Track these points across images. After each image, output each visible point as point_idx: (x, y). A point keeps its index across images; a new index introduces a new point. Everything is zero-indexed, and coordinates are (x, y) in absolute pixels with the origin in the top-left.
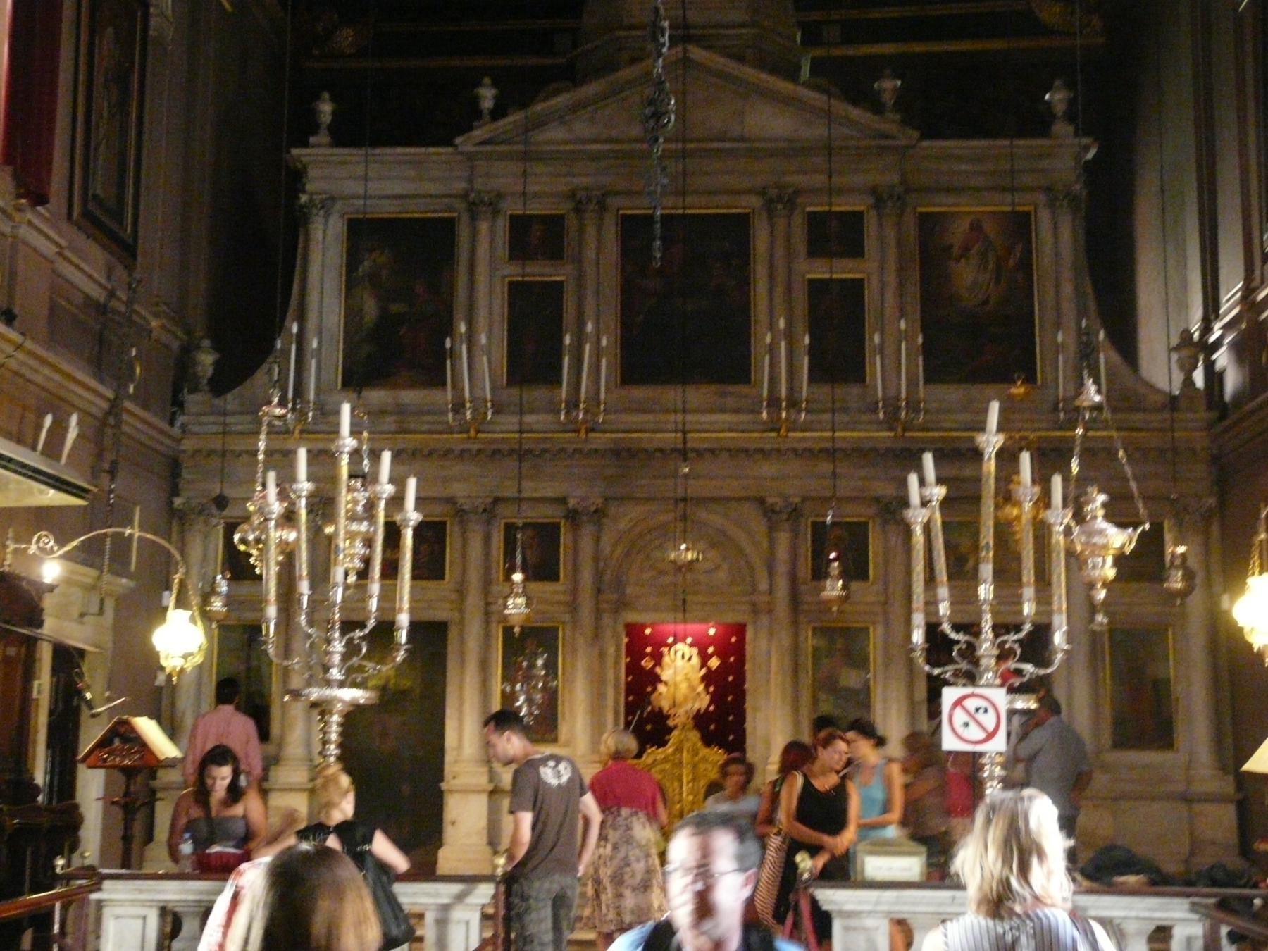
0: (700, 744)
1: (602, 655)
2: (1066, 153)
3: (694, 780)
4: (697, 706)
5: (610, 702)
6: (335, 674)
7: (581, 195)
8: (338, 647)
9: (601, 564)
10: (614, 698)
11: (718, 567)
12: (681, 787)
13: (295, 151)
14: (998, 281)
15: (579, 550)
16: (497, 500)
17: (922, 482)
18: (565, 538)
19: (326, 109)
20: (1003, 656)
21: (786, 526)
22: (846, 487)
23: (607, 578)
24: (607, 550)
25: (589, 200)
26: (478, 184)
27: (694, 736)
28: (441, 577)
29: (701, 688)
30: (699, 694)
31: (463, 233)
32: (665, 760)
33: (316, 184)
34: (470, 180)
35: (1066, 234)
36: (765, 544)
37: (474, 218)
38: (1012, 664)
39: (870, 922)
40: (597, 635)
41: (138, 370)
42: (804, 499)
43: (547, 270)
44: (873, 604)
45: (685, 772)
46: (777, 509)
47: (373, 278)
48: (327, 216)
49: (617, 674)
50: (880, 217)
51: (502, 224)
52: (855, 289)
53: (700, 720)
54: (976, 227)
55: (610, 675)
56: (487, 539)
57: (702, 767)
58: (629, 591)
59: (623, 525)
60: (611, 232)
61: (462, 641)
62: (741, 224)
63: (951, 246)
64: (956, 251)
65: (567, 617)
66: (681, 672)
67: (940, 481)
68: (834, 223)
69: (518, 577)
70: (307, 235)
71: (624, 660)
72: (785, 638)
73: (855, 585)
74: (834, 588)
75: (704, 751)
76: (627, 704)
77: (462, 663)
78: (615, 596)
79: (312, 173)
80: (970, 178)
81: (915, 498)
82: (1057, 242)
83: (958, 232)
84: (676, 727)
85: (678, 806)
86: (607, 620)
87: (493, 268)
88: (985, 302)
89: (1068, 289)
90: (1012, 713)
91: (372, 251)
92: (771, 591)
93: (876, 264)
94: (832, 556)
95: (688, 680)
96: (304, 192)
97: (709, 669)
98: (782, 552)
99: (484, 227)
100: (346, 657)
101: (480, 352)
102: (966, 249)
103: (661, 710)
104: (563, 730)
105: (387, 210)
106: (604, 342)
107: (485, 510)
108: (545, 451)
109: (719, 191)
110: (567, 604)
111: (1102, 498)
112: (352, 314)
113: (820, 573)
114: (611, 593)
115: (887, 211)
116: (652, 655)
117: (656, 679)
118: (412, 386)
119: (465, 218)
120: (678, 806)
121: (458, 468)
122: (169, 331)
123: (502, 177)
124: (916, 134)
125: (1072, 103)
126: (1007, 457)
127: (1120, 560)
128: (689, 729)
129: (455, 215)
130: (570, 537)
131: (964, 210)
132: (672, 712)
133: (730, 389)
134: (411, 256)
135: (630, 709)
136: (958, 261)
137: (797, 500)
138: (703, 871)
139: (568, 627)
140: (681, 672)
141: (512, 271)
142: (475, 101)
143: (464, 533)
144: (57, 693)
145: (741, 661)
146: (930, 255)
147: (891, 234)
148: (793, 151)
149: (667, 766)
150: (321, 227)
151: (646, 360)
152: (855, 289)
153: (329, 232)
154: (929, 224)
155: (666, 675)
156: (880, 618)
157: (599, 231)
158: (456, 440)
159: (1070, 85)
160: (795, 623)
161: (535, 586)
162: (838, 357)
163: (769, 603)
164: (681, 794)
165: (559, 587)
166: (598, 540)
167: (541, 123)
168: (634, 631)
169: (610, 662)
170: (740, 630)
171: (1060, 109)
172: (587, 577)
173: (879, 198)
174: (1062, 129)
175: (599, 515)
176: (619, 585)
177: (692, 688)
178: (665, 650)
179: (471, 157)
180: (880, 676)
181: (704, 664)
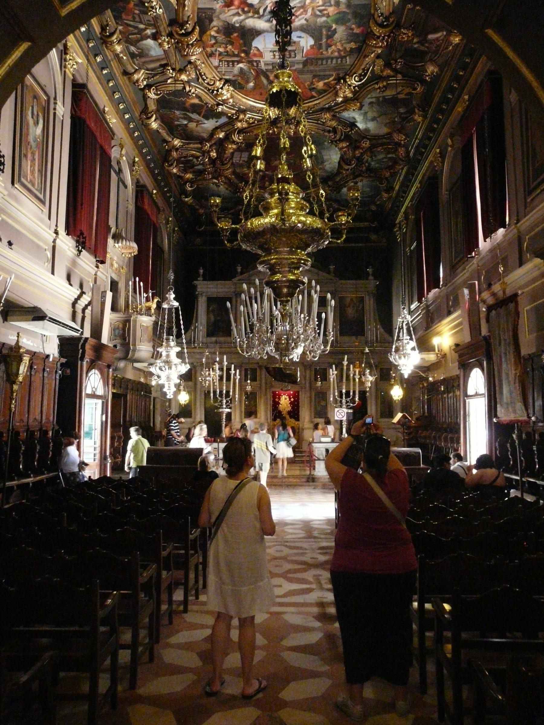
2: (372, 283)
5: (269, 409)
6: (224, 406)
8: (225, 401)
10: (270, 408)
13: (195, 282)
17: (333, 371)
19: (201, 271)
20: (347, 402)
35: (372, 302)
38: (348, 404)
39: (322, 449)
40: (266, 395)
47: (213, 311)
49: (270, 402)
53: (289, 413)
54: (352, 300)
64: (347, 305)
66: (285, 402)
67: (336, 370)
69: (249, 381)
70: (197, 301)
71: (272, 399)
72: (308, 394)
73: (324, 382)
74: (319, 383)
79: (199, 287)
81: (331, 374)
82: (370, 304)
83: (348, 300)
86: (268, 390)
88: (354, 317)
89: (372, 315)
90: (347, 413)
100: (226, 403)
104: (258, 415)
111: (368, 371)
112: (208, 319)
113: (316, 380)
117: (279, 403)
124: (338, 279)
125: (373, 271)
126: (348, 366)
127: (371, 383)
131: (350, 296)
135: (273, 411)
138: (203, 627)
140: (285, 402)
142: (236, 270)
145: (298, 399)
159: (372, 268)
161: (253, 383)
165: (258, 382)
170: (298, 392)
171: (371, 273)
172: (263, 381)
174: (371, 277)
177: (287, 405)
179: (236, 284)
181: (290, 400)
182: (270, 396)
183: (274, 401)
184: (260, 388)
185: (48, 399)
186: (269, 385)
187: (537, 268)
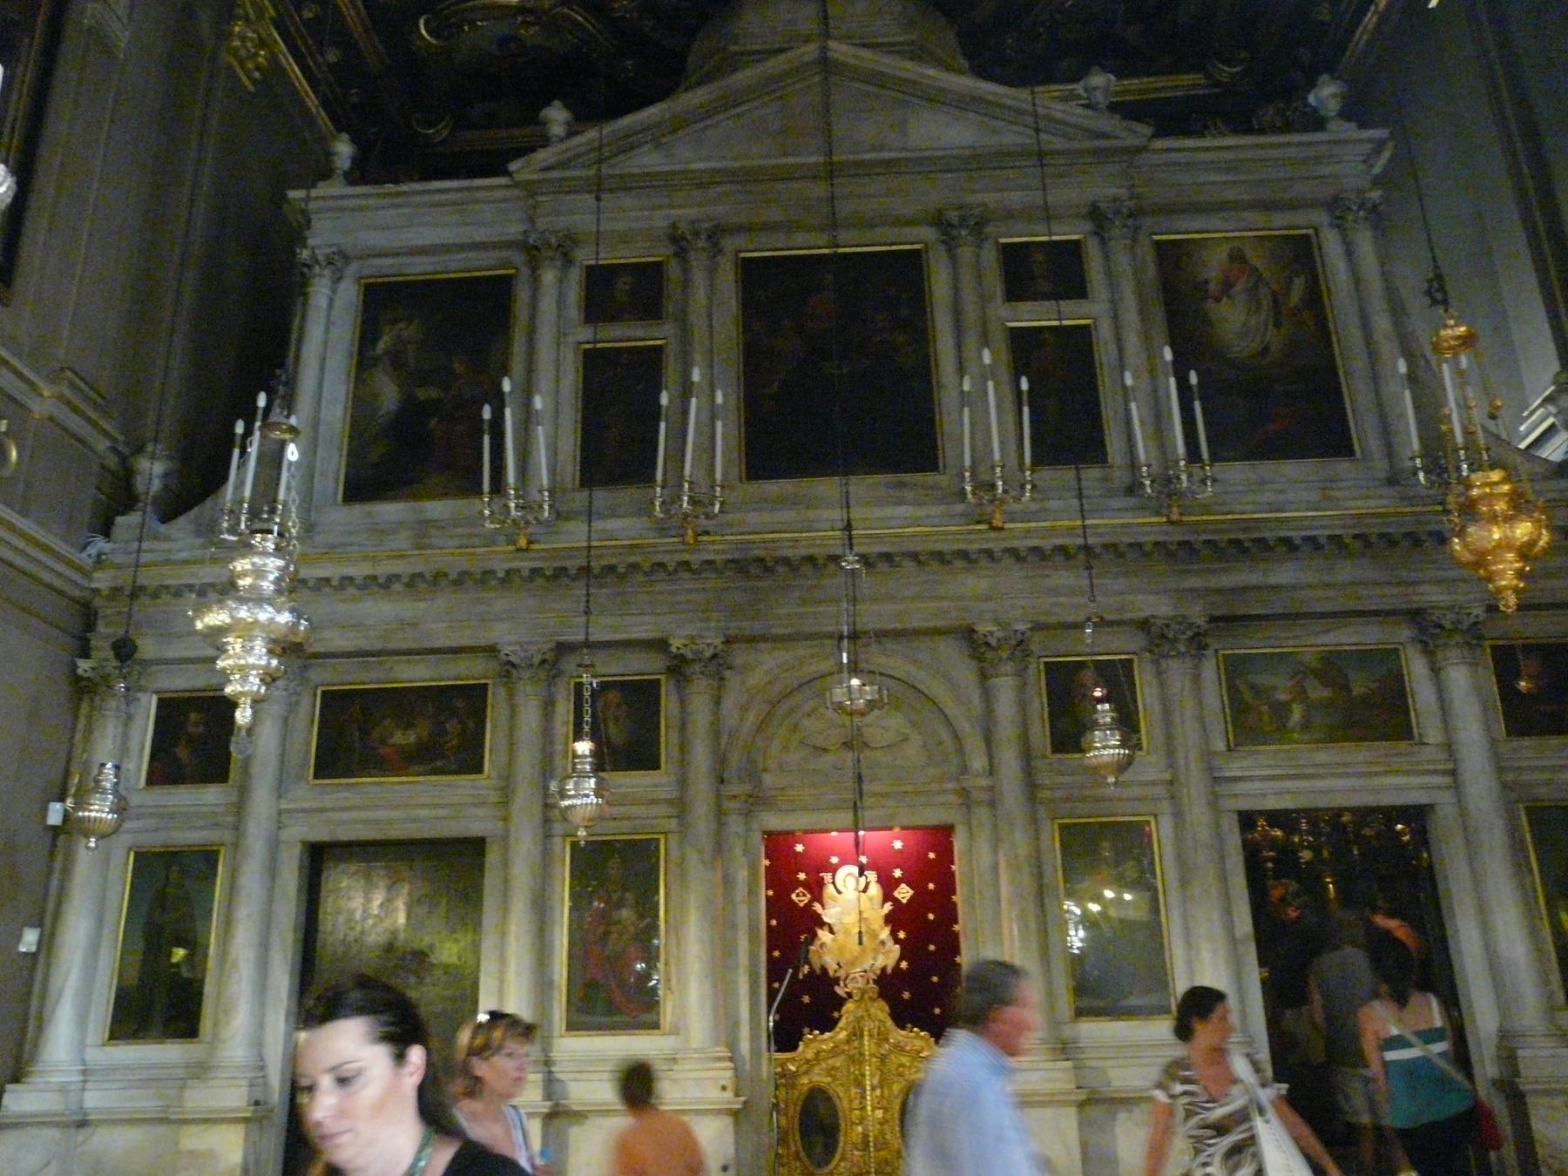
0: (890, 1023)
1: (728, 881)
3: (882, 1084)
4: (881, 962)
5: (743, 959)
7: (684, 228)
9: (724, 739)
10: (750, 952)
11: (906, 739)
12: (863, 1097)
14: (1277, 325)
15: (688, 716)
16: (563, 648)
18: (668, 703)
21: (1008, 667)
22: (1107, 603)
23: (735, 759)
25: (696, 234)
26: (542, 223)
27: (881, 1010)
28: (477, 768)
29: (885, 934)
30: (883, 943)
31: (522, 294)
32: (834, 1052)
33: (322, 237)
34: (532, 220)
37: (534, 266)
40: (719, 848)
41: (14, 454)
42: (1039, 627)
43: (640, 333)
44: (1154, 783)
45: (867, 1070)
46: (993, 642)
48: (337, 280)
49: (752, 912)
50: (1103, 242)
51: (575, 276)
52: (1078, 341)
53: (887, 984)
54: (1237, 257)
56: (548, 706)
57: (894, 1060)
58: (768, 779)
59: (756, 678)
60: (728, 278)
61: (505, 864)
62: (910, 267)
63: (1206, 282)
64: (1213, 287)
65: (673, 824)
66: (853, 910)
68: (1039, 257)
71: (763, 893)
75: (898, 1035)
76: (771, 960)
77: (505, 910)
78: (746, 788)
79: (317, 225)
80: (1224, 188)
83: (1213, 265)
85: (860, 1129)
86: (735, 824)
87: (561, 335)
88: (1265, 351)
91: (394, 322)
93: (1106, 306)
96: (305, 247)
97: (896, 901)
98: (1006, 707)
99: (549, 277)
101: (541, 419)
102: (1227, 286)
103: (824, 969)
104: (668, 1012)
105: (419, 268)
106: (719, 399)
107: (544, 661)
108: (634, 567)
109: (880, 223)
110: (670, 802)
112: (361, 402)
114: (741, 783)
115: (1116, 232)
116: (806, 885)
118: (445, 495)
119: (525, 271)
120: (860, 1129)
121: (500, 602)
122: (68, 403)
123: (577, 214)
128: (872, 1000)
129: (512, 271)
130: (674, 699)
131: (1216, 238)
132: (842, 973)
133: (906, 477)
134: (445, 338)
136: (1218, 300)
137: (1021, 627)
140: (853, 910)
141: (584, 334)
143: (511, 695)
146: (1179, 300)
147: (1122, 262)
148: (975, 162)
149: (838, 1062)
150: (326, 291)
151: (783, 441)
152: (1078, 341)
153: (338, 303)
154: (1172, 257)
155: (829, 915)
156: (1166, 806)
158: (500, 559)
160: (1035, 822)
162: (1067, 424)
163: (992, 788)
164: (863, 1109)
166: (718, 702)
167: (627, 144)
168: (777, 844)
170: (941, 837)
171: (1333, 106)
172: (701, 758)
173: (1097, 217)
175: (718, 665)
176: (752, 773)
178: (827, 877)
179: (532, 190)
180: (1174, 897)
181: (888, 896)
182: (749, 870)
183: (779, 905)
184: (681, 807)
186: (737, 788)
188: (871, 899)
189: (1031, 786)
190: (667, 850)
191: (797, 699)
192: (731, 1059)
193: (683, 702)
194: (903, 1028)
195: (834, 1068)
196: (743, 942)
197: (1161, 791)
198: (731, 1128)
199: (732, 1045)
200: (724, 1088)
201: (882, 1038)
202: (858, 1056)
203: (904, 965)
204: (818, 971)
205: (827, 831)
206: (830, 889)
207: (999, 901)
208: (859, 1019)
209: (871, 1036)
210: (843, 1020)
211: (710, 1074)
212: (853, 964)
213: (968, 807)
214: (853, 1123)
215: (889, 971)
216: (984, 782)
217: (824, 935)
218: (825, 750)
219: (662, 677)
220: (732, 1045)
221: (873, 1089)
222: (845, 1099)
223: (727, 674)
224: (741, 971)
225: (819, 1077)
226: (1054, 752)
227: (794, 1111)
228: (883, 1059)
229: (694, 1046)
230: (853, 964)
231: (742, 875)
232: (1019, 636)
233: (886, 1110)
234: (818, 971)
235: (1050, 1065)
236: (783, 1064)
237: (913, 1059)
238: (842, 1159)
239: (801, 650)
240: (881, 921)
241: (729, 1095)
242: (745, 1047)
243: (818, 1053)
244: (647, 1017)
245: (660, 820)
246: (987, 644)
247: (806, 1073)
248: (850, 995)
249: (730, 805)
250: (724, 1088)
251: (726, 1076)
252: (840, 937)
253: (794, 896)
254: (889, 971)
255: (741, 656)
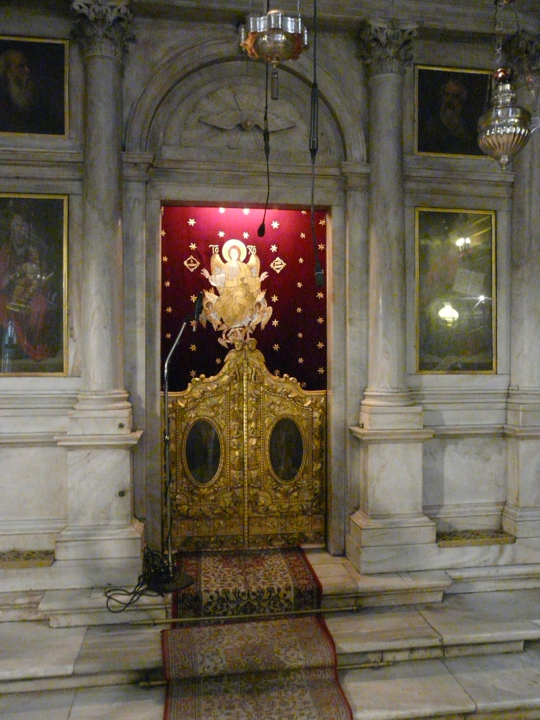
0: (265, 369)
1: (128, 242)
3: (257, 418)
4: (256, 320)
5: (141, 313)
11: (292, 128)
12: (241, 428)
18: (73, 70)
23: (136, 128)
24: (136, 92)
27: (257, 359)
29: (261, 297)
30: (259, 304)
32: (217, 392)
36: (359, 95)
40: (120, 209)
42: (425, 33)
44: (497, 184)
46: (383, 39)
49: (148, 271)
53: (262, 337)
55: (140, 272)
57: (267, 399)
59: (159, 55)
65: (75, 187)
66: (235, 278)
71: (159, 259)
75: (271, 380)
84: (231, 346)
85: (237, 453)
86: (136, 190)
92: (369, 159)
94: (499, 70)
95: (245, 285)
97: (272, 272)
103: (209, 324)
104: (71, 353)
116: (196, 253)
132: (224, 328)
135: (169, 324)
139: (76, 202)
140: (235, 278)
144: (326, 434)
155: (216, 279)
156: (505, 204)
157: (121, 71)
160: (402, 205)
163: (367, 177)
166: (121, 71)
169: (140, 255)
176: (152, 142)
177: (250, 297)
180: (504, 280)
181: (265, 266)
182: (147, 234)
183: (172, 270)
184: (82, 168)
185: (312, 549)
186: (139, 156)
187: (408, 390)
188: (251, 268)
189: (403, 177)
190: (72, 211)
191: (196, 79)
192: (128, 399)
193: (86, 69)
194: (273, 373)
195: (218, 405)
196: (141, 297)
197: (502, 191)
198: (128, 461)
199: (130, 388)
200: (121, 426)
201: (258, 381)
202: (244, 401)
203: (275, 323)
204: (204, 325)
205: (216, 205)
206: (216, 258)
207: (367, 272)
208: (239, 366)
209: (249, 380)
210: (226, 366)
211: (111, 413)
212: (235, 319)
213: (345, 192)
214: (231, 449)
215: (263, 327)
216: (362, 169)
217: (210, 296)
218: (222, 130)
219: (66, 43)
220: (130, 388)
221: (249, 421)
222: (223, 426)
223: (131, 47)
224: (138, 323)
225: (203, 412)
226: (422, 148)
227: (182, 440)
228: (258, 399)
229: (94, 388)
230: (235, 319)
231: (142, 237)
232: (406, 36)
233: (259, 438)
234: (204, 325)
235: (405, 409)
236: (174, 401)
237: (283, 399)
238: (222, 475)
239: (203, 32)
240: (259, 287)
241: (126, 431)
242: (141, 389)
243: (203, 394)
244: (51, 361)
245: (60, 182)
246: (376, 40)
247: (193, 409)
248: (231, 346)
249: (130, 172)
250: (121, 426)
251: (124, 415)
252: (224, 298)
253: (185, 263)
254: (263, 327)
255: (143, 30)
